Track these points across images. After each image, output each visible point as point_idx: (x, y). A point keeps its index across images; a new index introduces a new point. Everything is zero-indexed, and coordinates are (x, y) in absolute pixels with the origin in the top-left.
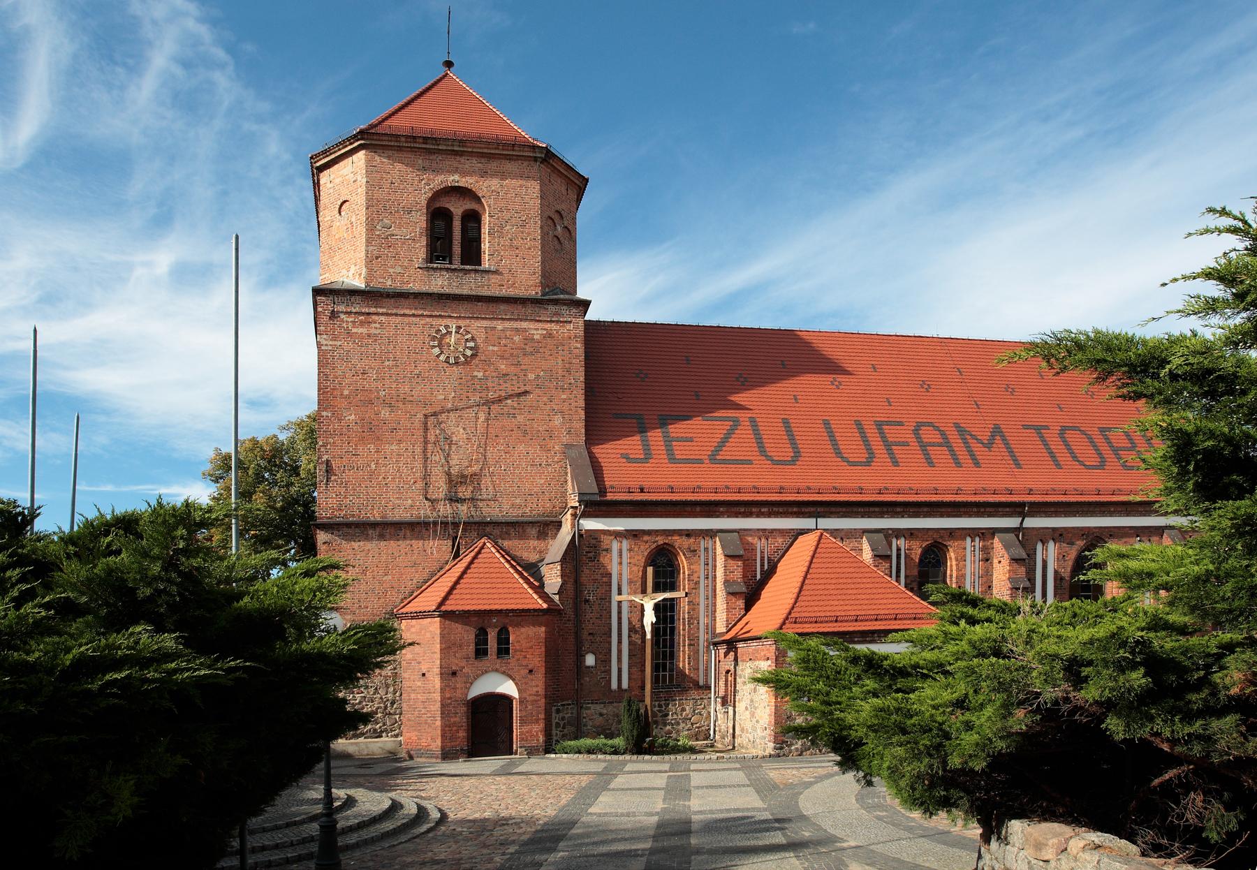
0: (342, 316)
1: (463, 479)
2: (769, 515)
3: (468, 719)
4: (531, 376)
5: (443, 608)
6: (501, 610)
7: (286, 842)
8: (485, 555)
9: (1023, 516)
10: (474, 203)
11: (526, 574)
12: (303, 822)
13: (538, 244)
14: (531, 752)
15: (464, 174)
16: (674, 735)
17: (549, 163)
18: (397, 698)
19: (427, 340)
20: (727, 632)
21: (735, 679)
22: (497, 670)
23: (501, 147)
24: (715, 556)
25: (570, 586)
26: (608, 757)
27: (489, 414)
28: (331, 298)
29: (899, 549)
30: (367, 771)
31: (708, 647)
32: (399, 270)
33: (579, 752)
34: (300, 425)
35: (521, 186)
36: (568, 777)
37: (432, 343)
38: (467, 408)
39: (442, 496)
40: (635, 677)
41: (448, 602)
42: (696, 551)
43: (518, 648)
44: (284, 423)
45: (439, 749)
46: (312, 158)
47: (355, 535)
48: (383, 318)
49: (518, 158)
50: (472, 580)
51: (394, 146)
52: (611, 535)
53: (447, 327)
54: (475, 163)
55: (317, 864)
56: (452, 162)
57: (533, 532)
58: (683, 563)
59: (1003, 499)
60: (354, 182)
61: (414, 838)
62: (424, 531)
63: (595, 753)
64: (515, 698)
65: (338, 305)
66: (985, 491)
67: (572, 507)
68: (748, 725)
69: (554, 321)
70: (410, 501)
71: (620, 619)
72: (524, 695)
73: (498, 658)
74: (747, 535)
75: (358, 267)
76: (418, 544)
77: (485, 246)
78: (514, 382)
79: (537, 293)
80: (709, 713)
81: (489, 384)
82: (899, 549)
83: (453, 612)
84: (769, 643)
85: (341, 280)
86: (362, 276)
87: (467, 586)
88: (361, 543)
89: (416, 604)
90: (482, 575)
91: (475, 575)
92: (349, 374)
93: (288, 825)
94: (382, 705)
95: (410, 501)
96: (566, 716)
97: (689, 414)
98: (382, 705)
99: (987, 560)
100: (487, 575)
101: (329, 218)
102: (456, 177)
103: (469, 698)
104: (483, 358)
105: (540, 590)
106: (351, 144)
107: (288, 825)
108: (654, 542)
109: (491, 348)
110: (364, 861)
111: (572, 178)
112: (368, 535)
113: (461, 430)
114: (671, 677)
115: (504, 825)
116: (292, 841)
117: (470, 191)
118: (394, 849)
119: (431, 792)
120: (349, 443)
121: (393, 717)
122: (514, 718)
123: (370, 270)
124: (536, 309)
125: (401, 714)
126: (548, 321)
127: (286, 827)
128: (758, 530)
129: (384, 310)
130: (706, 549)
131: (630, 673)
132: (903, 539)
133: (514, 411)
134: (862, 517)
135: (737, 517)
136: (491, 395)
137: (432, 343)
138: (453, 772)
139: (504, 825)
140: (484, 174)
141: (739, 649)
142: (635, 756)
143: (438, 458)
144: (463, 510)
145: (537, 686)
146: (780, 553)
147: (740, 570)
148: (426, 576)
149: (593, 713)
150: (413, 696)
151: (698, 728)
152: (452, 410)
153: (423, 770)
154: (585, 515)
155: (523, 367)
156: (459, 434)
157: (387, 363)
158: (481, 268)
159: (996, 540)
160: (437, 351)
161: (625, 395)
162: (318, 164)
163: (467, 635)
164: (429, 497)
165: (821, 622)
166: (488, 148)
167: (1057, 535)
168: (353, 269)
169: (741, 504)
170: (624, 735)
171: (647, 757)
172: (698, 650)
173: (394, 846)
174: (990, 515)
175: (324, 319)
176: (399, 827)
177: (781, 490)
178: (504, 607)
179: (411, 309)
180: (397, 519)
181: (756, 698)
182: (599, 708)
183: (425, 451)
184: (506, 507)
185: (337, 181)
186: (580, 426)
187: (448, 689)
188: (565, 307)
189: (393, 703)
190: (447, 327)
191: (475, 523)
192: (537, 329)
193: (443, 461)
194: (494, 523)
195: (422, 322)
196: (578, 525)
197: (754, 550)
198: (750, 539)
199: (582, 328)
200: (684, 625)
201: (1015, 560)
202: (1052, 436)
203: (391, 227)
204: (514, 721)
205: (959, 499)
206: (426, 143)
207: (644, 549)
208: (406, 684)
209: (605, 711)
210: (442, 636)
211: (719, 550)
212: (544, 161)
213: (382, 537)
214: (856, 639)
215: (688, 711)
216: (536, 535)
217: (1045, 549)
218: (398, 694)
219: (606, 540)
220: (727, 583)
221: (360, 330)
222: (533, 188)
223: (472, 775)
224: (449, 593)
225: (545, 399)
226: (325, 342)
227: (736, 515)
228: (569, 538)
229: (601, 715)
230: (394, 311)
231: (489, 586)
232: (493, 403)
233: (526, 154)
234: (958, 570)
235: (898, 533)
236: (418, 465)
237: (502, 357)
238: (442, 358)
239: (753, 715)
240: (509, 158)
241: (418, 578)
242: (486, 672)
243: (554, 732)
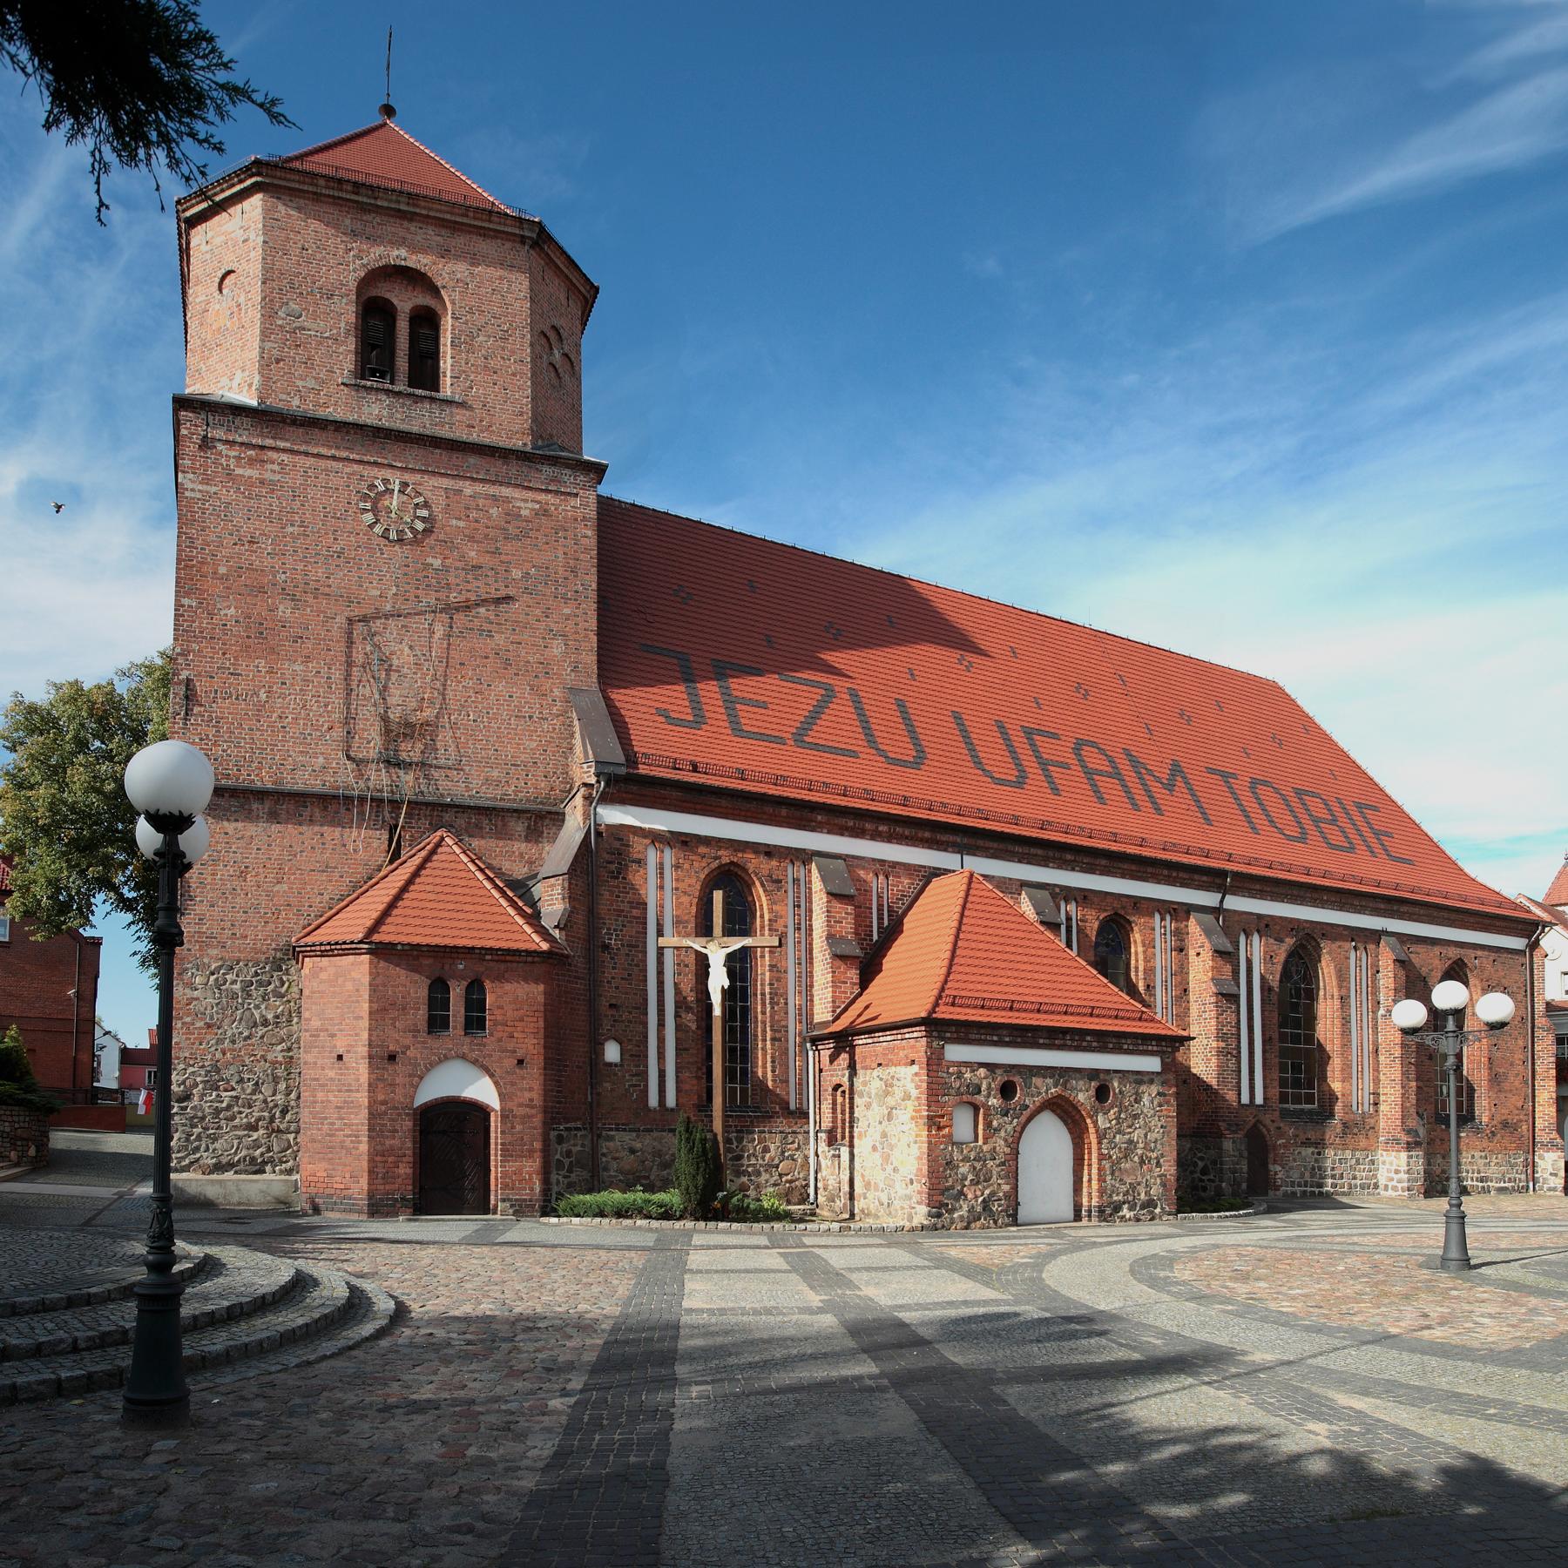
0: (220, 447)
1: (409, 730)
2: (890, 838)
3: (414, 1142)
4: (517, 573)
5: (376, 938)
6: (473, 948)
7: (61, 1341)
8: (443, 857)
9: (1224, 891)
10: (428, 297)
11: (510, 894)
12: (107, 1298)
13: (527, 369)
14: (521, 1210)
15: (414, 249)
16: (752, 1193)
17: (542, 249)
18: (292, 1103)
19: (354, 499)
20: (834, 1021)
21: (852, 1099)
22: (463, 1057)
23: (471, 214)
24: (811, 893)
25: (580, 918)
26: (655, 1224)
27: (451, 627)
28: (203, 416)
29: (1069, 919)
30: (239, 1229)
31: (802, 1045)
32: (311, 383)
33: (602, 1214)
34: (149, 669)
35: (501, 278)
36: (602, 1253)
37: (361, 505)
38: (416, 614)
39: (373, 754)
40: (686, 1087)
41: (384, 928)
42: (780, 881)
43: (499, 1018)
44: (125, 665)
45: (364, 1195)
46: (178, 202)
47: (228, 810)
48: (285, 457)
49: (497, 235)
50: (421, 896)
51: (308, 192)
52: (645, 837)
53: (386, 481)
54: (431, 234)
55: (128, 1400)
56: (393, 228)
57: (519, 827)
58: (760, 901)
59: (1200, 862)
60: (245, 241)
61: (351, 1348)
62: (343, 810)
63: (630, 1217)
64: (493, 1110)
65: (213, 428)
66: (1174, 848)
67: (585, 785)
68: (878, 1177)
69: (550, 491)
70: (321, 760)
71: (661, 983)
72: (510, 1105)
73: (466, 1034)
74: (857, 866)
75: (247, 373)
76: (332, 833)
77: (446, 364)
78: (491, 581)
79: (525, 444)
80: (806, 1158)
81: (452, 580)
82: (1069, 919)
83: (392, 945)
84: (915, 1035)
85: (221, 392)
86: (254, 388)
87: (415, 904)
88: (240, 825)
89: (329, 931)
90: (439, 889)
91: (429, 888)
92: (228, 541)
93: (71, 1303)
94: (266, 1114)
95: (321, 760)
96: (575, 1149)
97: (761, 666)
98: (266, 1114)
99: (1181, 950)
100: (448, 889)
101: (203, 298)
102: (403, 252)
103: (416, 1105)
104: (442, 537)
105: (534, 919)
106: (241, 181)
107: (71, 1303)
108: (716, 858)
109: (454, 522)
110: (243, 1398)
111: (575, 281)
112: (250, 811)
113: (406, 649)
114: (744, 1091)
115: (531, 1329)
116: (75, 1340)
117: (424, 275)
118: (310, 1371)
119: (362, 1264)
120: (224, 654)
121: (285, 1136)
122: (492, 1146)
123: (266, 380)
124: (524, 469)
125: (297, 1132)
126: (542, 490)
127: (66, 1308)
128: (874, 860)
129: (288, 445)
130: (796, 881)
131: (678, 1081)
132: (1074, 904)
133: (489, 627)
134: (1020, 862)
135: (842, 835)
136: (453, 597)
137: (361, 505)
138: (392, 1236)
139: (531, 1329)
140: (445, 253)
141: (858, 1050)
142: (702, 1224)
143: (368, 690)
144: (408, 782)
145: (531, 1089)
146: (907, 901)
147: (850, 919)
148: (344, 889)
149: (620, 1144)
150: (320, 1096)
151: (790, 1182)
152: (393, 616)
153: (338, 1230)
154: (606, 799)
155: (503, 557)
156: (403, 656)
157: (291, 529)
158: (441, 395)
159: (1192, 923)
160: (369, 518)
161: (657, 619)
162: (188, 214)
163: (415, 988)
164: (352, 754)
165: (990, 1008)
166: (452, 213)
167: (1262, 925)
168: (238, 379)
169: (850, 813)
170: (680, 1185)
171: (722, 1225)
172: (787, 1049)
173: (309, 1363)
174: (1184, 885)
175: (191, 448)
176: (317, 1321)
177: (905, 802)
178: (478, 944)
179: (330, 447)
180: (299, 787)
181: (891, 1129)
182: (627, 1138)
183: (348, 677)
184: (476, 783)
185: (218, 241)
186: (590, 659)
187: (381, 1085)
188: (568, 472)
189: (284, 1112)
190: (386, 481)
191: (427, 804)
192: (526, 501)
193: (377, 696)
194: (457, 806)
195: (348, 470)
196: (595, 814)
197: (868, 892)
198: (862, 873)
199: (593, 506)
200: (764, 1004)
201: (1219, 953)
202: (1242, 785)
203: (300, 316)
204: (492, 1152)
205: (1146, 852)
206: (357, 194)
207: (699, 869)
208: (308, 1073)
209: (638, 1145)
210: (373, 987)
211: (817, 885)
212: (535, 245)
213: (274, 817)
214: (1041, 1041)
215: (773, 1153)
216: (523, 834)
217: (1249, 944)
218: (293, 1096)
219: (637, 844)
220: (830, 937)
221: (248, 472)
222: (519, 284)
223: (428, 1243)
224: (386, 913)
225: (538, 612)
226: (190, 486)
227: (841, 831)
228: (579, 837)
229: (632, 1151)
230: (303, 448)
231: (451, 906)
232: (457, 609)
233: (509, 230)
234: (1146, 960)
235: (1068, 894)
236: (337, 700)
237: (472, 539)
238: (378, 529)
239: (886, 1159)
240: (484, 233)
241: (332, 891)
242: (446, 1058)
243: (554, 1177)
